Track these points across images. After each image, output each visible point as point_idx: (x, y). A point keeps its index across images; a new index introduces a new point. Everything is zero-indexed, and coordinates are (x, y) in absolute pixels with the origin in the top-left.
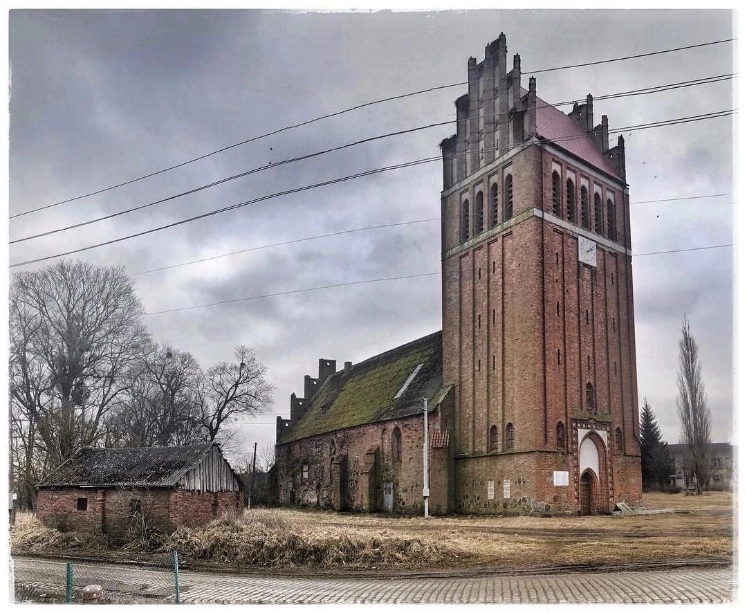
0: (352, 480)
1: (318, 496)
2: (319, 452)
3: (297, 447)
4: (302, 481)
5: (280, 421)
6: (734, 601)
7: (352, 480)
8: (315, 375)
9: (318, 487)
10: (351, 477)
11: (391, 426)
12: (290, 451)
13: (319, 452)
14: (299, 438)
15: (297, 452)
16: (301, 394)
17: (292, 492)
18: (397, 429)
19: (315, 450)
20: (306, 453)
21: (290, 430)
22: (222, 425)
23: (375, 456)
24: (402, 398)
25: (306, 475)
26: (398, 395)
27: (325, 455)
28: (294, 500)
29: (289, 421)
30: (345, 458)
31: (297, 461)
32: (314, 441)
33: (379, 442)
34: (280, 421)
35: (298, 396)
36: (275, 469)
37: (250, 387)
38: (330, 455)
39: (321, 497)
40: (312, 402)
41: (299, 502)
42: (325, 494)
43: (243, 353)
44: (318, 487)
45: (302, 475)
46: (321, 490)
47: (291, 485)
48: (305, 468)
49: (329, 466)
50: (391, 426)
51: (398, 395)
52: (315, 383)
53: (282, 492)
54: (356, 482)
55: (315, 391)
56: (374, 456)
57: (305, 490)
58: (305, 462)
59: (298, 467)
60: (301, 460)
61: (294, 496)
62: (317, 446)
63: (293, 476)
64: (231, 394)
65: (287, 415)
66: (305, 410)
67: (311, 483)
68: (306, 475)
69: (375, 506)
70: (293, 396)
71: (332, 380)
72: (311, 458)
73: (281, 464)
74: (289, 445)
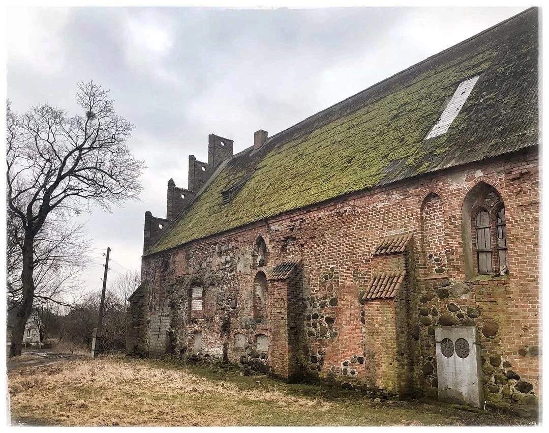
0: (315, 316)
1: (225, 345)
2: (227, 262)
3: (180, 257)
4: (189, 315)
5: (150, 220)
6: (539, 425)
7: (315, 316)
8: (203, 157)
9: (226, 328)
10: (309, 311)
11: (462, 184)
12: (166, 265)
13: (227, 262)
14: (183, 242)
15: (180, 266)
16: (183, 183)
17: (170, 334)
18: (484, 190)
19: (217, 260)
20: (198, 267)
21: (164, 234)
22: (50, 216)
23: (407, 260)
24: (456, 134)
25: (197, 305)
26: (441, 128)
27: (240, 267)
28: (173, 347)
29: (164, 220)
30: (297, 269)
31: (180, 281)
32: (215, 244)
33: (413, 226)
34: (150, 220)
35: (178, 185)
36: (137, 298)
37: (106, 157)
38: (254, 267)
39: (231, 346)
40: (200, 196)
41: (182, 351)
42: (242, 342)
43: (92, 95)
44: (226, 328)
45: (190, 305)
46: (232, 333)
47: (167, 322)
48: (197, 292)
49: (250, 289)
50: (462, 184)
51: (441, 128)
52: (203, 169)
53: (150, 333)
54: (330, 321)
55: (203, 182)
56: (402, 260)
57: (196, 332)
58: (196, 283)
59: (183, 291)
60: (188, 279)
61: (173, 340)
62: (220, 254)
63: (173, 306)
64: (70, 164)
65: (161, 212)
66: (189, 208)
67: (209, 320)
68: (197, 305)
69: (410, 381)
70: (171, 183)
71: (229, 165)
72: (207, 274)
73: (150, 287)
74: (166, 254)
